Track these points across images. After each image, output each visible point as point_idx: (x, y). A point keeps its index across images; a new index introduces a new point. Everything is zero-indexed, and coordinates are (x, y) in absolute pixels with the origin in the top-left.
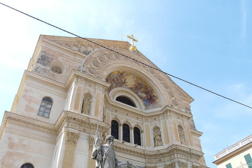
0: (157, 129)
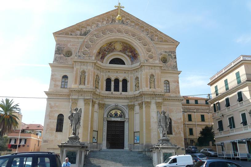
0: (137, 78)
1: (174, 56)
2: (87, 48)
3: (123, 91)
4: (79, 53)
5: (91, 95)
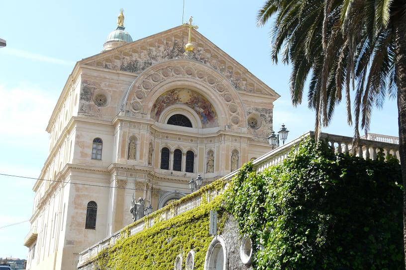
0: (211, 153)
1: (269, 119)
2: (138, 98)
3: (174, 169)
4: (128, 107)
5: (145, 177)
